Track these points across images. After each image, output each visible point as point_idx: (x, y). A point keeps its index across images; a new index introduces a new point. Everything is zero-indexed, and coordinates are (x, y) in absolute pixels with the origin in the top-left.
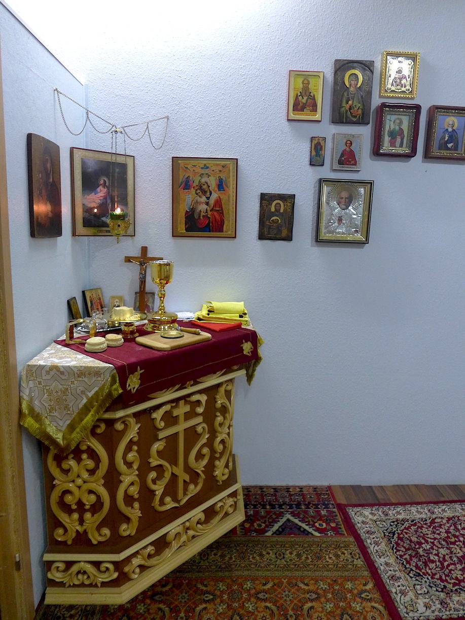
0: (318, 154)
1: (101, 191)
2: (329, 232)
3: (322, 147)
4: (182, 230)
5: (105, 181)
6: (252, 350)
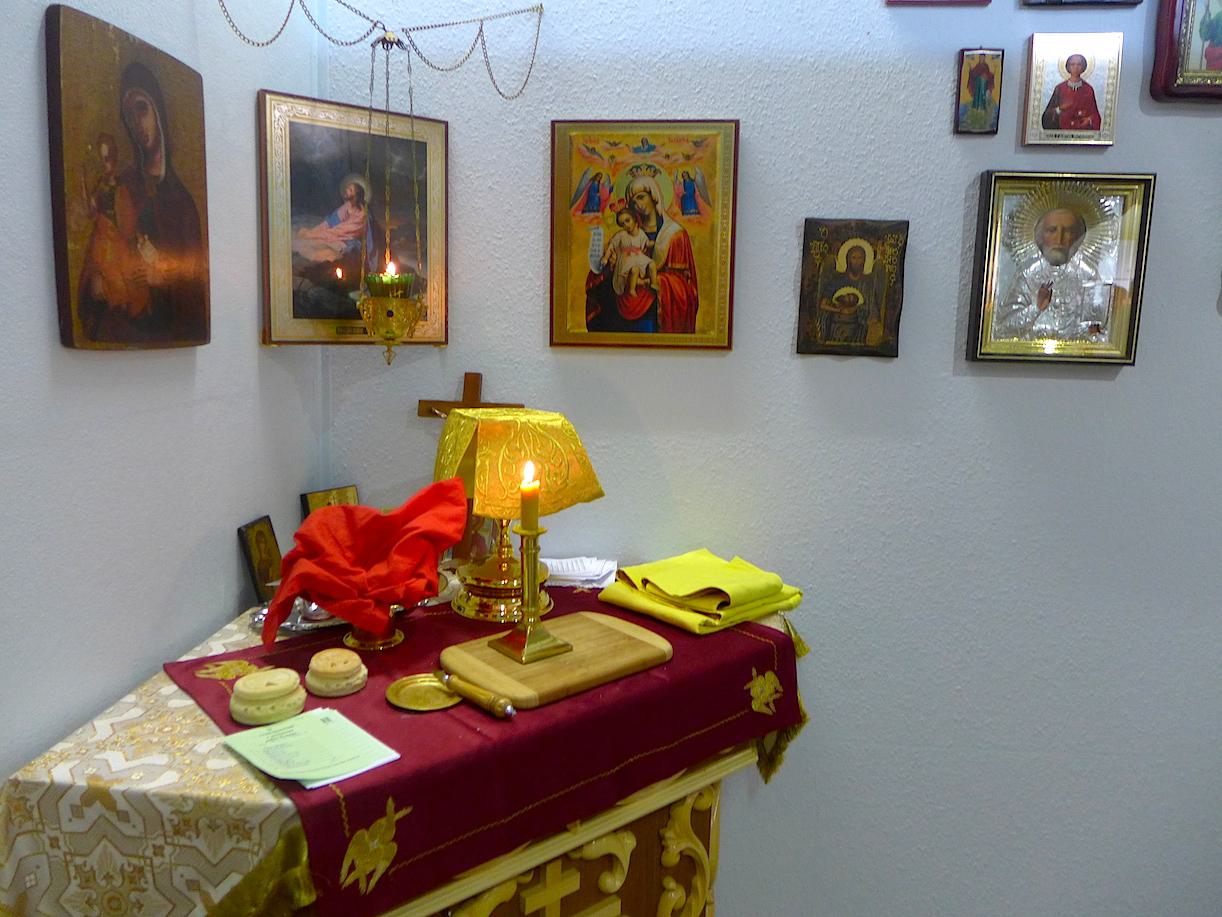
0: (979, 100)
1: (348, 216)
2: (1012, 332)
3: (991, 78)
4: (579, 326)
5: (358, 187)
6: (778, 696)
